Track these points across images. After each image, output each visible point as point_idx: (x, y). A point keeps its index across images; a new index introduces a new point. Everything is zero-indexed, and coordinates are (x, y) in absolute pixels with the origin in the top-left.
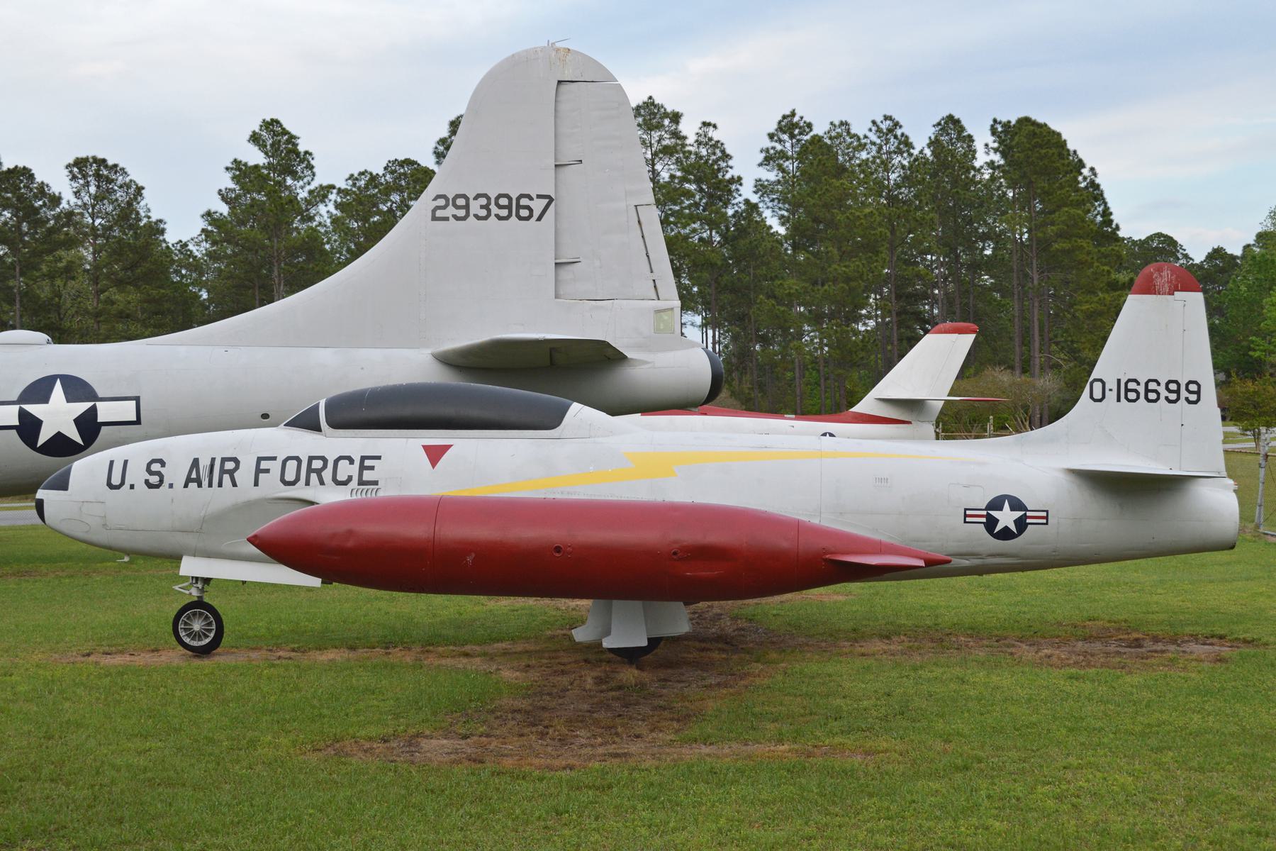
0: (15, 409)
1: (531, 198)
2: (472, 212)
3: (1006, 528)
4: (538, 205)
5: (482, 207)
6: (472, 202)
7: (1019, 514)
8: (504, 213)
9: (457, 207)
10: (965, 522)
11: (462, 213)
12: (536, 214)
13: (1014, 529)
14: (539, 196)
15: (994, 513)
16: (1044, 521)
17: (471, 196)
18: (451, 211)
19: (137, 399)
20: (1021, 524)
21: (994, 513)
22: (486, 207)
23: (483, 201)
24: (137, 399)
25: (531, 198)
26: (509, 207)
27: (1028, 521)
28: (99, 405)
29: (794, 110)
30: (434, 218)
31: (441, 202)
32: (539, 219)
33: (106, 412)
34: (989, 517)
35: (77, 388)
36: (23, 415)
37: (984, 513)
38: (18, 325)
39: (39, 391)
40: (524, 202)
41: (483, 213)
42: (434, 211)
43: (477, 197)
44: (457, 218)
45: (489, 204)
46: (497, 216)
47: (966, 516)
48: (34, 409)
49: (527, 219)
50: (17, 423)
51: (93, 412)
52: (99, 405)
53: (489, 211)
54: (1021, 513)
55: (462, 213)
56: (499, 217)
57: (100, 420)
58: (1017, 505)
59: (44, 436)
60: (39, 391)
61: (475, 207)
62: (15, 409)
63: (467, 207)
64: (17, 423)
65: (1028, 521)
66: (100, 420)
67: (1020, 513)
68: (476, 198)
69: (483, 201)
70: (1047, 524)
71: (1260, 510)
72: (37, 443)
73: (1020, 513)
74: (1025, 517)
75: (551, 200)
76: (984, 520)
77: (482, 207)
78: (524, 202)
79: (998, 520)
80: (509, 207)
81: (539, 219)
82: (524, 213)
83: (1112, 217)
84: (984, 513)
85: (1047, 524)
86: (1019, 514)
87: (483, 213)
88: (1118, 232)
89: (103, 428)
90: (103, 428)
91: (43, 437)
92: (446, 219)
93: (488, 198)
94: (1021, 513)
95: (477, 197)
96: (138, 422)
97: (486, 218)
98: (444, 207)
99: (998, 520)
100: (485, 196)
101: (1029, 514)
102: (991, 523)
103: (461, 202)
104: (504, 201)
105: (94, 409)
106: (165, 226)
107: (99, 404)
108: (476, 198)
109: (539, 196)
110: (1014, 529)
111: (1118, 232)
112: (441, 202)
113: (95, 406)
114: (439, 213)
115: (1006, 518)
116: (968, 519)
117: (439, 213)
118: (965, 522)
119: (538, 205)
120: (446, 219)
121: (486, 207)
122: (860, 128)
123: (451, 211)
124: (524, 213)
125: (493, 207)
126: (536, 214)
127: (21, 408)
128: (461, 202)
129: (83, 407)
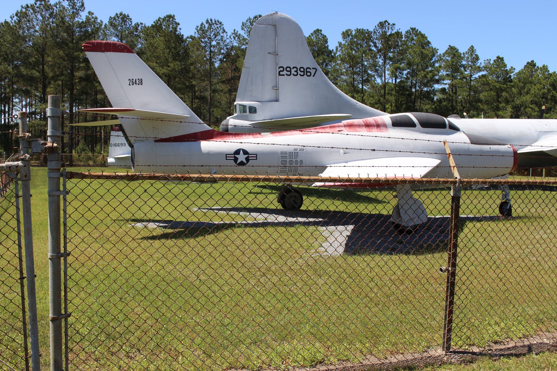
2: (292, 73)
3: (242, 162)
4: (313, 71)
5: (295, 71)
6: (292, 69)
7: (247, 156)
9: (288, 71)
10: (226, 159)
15: (237, 156)
16: (255, 158)
17: (292, 68)
20: (247, 159)
21: (237, 156)
22: (296, 71)
23: (295, 69)
26: (307, 72)
27: (250, 158)
30: (280, 75)
31: (282, 69)
32: (314, 76)
34: (235, 157)
37: (233, 156)
40: (308, 70)
41: (295, 73)
43: (294, 68)
44: (287, 75)
47: (226, 157)
49: (310, 76)
54: (247, 156)
55: (289, 73)
56: (301, 75)
58: (245, 152)
61: (293, 71)
63: (290, 71)
65: (250, 158)
67: (247, 156)
68: (293, 68)
69: (295, 69)
70: (256, 159)
71: (5, 116)
73: (247, 156)
74: (248, 157)
76: (233, 158)
77: (295, 71)
80: (304, 72)
81: (314, 76)
83: (344, 31)
84: (233, 156)
85: (256, 159)
86: (247, 156)
87: (295, 73)
89: (469, 229)
92: (284, 75)
93: (297, 69)
94: (247, 156)
95: (294, 68)
98: (283, 71)
100: (296, 67)
101: (250, 156)
102: (236, 160)
103: (288, 69)
108: (293, 68)
112: (282, 69)
114: (281, 73)
115: (242, 157)
116: (227, 158)
117: (281, 73)
118: (226, 159)
120: (284, 75)
121: (296, 71)
124: (309, 74)
125: (299, 71)
128: (288, 69)
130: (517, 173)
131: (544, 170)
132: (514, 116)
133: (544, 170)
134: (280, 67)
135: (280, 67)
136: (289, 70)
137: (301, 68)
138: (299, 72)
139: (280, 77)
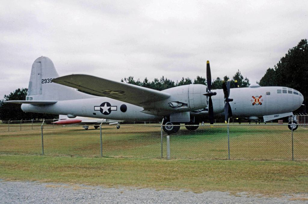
0: (99, 107)
11: (46, 82)
19: (117, 106)
22: (49, 81)
23: (48, 80)
24: (117, 106)
28: (111, 107)
30: (42, 83)
31: (43, 80)
33: (112, 108)
34: (101, 108)
35: (109, 105)
36: (101, 108)
38: (272, 84)
41: (48, 82)
43: (48, 79)
48: (102, 107)
50: (100, 109)
51: (110, 108)
52: (111, 107)
55: (46, 82)
59: (104, 112)
60: (103, 105)
62: (99, 107)
63: (46, 81)
64: (100, 109)
69: (48, 80)
87: (48, 82)
88: (285, 57)
89: (112, 111)
91: (104, 112)
95: (48, 79)
96: (117, 110)
98: (43, 81)
106: (276, 66)
111: (285, 57)
112: (43, 80)
114: (43, 82)
117: (43, 82)
121: (49, 81)
123: (44, 82)
125: (50, 81)
128: (46, 80)
129: (109, 107)
130: (292, 49)
131: (207, 112)
132: (272, 84)
133: (207, 112)
134: (42, 80)
135: (42, 80)
136: (46, 80)
137: (51, 79)
138: (50, 81)
139: (117, 110)
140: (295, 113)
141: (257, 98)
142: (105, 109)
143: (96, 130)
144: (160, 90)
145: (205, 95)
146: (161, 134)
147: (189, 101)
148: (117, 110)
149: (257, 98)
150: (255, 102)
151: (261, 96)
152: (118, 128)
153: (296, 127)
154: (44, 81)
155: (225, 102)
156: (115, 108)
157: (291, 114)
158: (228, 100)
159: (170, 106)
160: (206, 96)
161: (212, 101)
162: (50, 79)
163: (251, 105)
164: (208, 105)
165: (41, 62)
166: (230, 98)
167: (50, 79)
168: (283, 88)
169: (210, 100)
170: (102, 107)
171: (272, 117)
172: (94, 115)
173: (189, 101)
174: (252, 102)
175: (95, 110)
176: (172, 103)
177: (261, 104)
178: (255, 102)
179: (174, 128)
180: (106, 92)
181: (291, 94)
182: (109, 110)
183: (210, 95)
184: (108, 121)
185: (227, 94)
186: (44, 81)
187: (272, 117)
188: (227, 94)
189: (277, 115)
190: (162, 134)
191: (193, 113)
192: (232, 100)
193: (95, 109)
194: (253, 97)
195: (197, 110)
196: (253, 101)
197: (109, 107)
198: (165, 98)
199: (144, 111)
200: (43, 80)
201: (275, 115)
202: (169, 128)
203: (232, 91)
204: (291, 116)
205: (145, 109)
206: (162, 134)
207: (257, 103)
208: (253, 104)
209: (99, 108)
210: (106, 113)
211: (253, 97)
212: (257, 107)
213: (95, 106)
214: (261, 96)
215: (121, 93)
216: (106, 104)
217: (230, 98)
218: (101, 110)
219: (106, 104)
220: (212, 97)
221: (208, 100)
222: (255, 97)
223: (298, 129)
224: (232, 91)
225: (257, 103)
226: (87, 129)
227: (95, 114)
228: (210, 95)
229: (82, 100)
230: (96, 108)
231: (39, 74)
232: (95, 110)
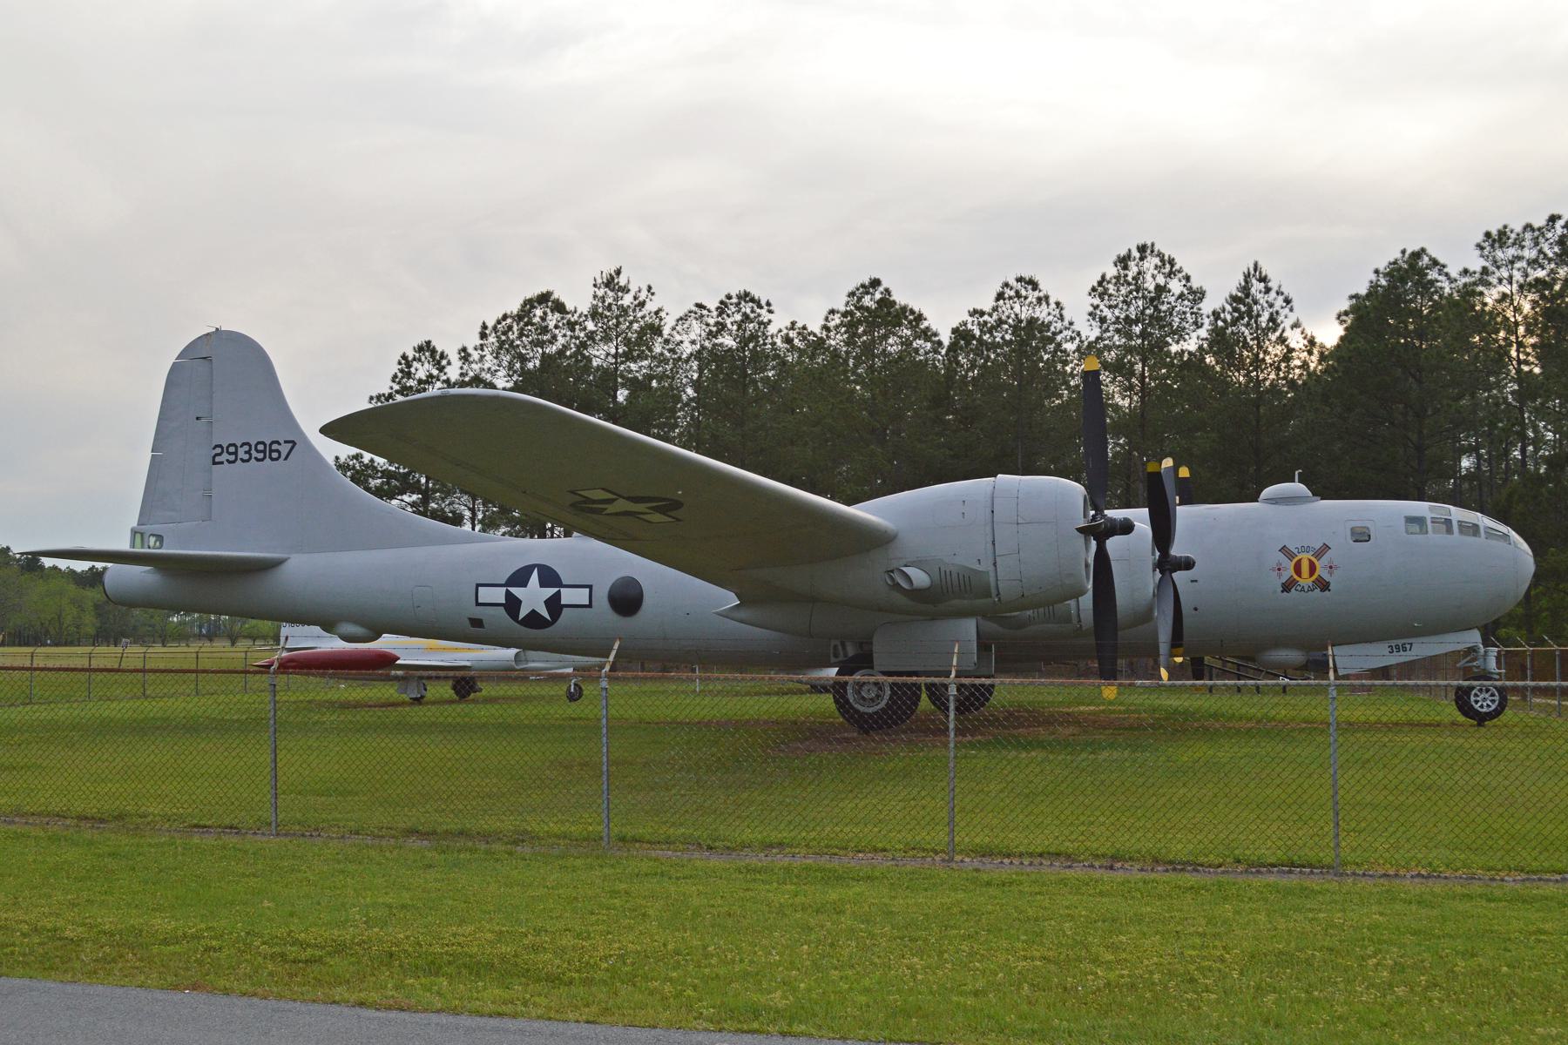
1: (279, 444)
4: (284, 449)
5: (246, 452)
8: (260, 456)
9: (230, 454)
11: (232, 458)
12: (283, 456)
13: (545, 614)
14: (286, 442)
17: (239, 445)
18: (225, 457)
23: (246, 448)
24: (590, 587)
25: (279, 444)
29: (484, 323)
31: (218, 450)
32: (286, 459)
33: (568, 596)
35: (549, 577)
36: (509, 595)
39: (520, 578)
40: (275, 447)
41: (246, 457)
42: (214, 457)
43: (243, 444)
45: (250, 449)
46: (256, 458)
48: (514, 590)
51: (558, 595)
53: (250, 455)
55: (232, 458)
56: (257, 459)
57: (562, 603)
59: (523, 613)
60: (520, 578)
61: (242, 454)
63: (236, 453)
66: (562, 603)
69: (246, 448)
72: (518, 616)
75: (294, 443)
77: (246, 452)
78: (275, 447)
79: (533, 611)
80: (264, 452)
81: (286, 459)
82: (275, 455)
87: (246, 457)
89: (565, 609)
90: (565, 609)
91: (523, 613)
92: (222, 463)
95: (243, 444)
96: (590, 606)
97: (248, 461)
98: (220, 454)
99: (533, 611)
100: (248, 444)
103: (232, 449)
104: (261, 447)
105: (558, 595)
107: (562, 589)
109: (286, 442)
110: (545, 614)
112: (218, 450)
113: (559, 592)
114: (217, 459)
117: (217, 459)
119: (284, 449)
120: (222, 463)
122: (671, 304)
123: (225, 457)
125: (253, 452)
126: (283, 456)
127: (507, 591)
128: (232, 449)
129: (553, 591)
135: (216, 446)
140: (1490, 633)
141: (1305, 558)
142: (533, 596)
143: (460, 707)
144: (849, 502)
145: (1080, 530)
146: (947, 729)
147: (995, 564)
148: (590, 606)
149: (1305, 558)
150: (1296, 577)
151: (1326, 547)
152: (574, 697)
153: (1497, 698)
154: (226, 453)
155: (1154, 570)
156: (581, 596)
157: (1474, 638)
158: (1167, 564)
159: (897, 586)
160: (1081, 538)
161: (1113, 563)
162: (268, 443)
163: (1275, 592)
164: (1090, 586)
165: (214, 359)
166: (1176, 551)
167: (268, 443)
168: (1431, 509)
169: (1102, 558)
170: (514, 590)
171: (1379, 655)
172: (475, 631)
173: (995, 564)
174: (1280, 576)
175: (478, 604)
176: (904, 569)
177: (1324, 586)
178: (1296, 577)
179: (894, 693)
180: (588, 500)
181: (1476, 539)
182: (554, 604)
183: (1100, 532)
184: (527, 661)
185: (1163, 530)
186: (226, 453)
187: (1379, 655)
188: (1163, 530)
189: (1400, 642)
190: (952, 726)
191: (991, 627)
192: (1188, 564)
193: (480, 601)
194: (1284, 550)
195: (1008, 614)
196: (1286, 569)
197: (553, 591)
198: (872, 540)
199: (742, 614)
200: (220, 446)
201: (1394, 642)
202: (872, 700)
203: (1186, 515)
204: (1472, 650)
205: (745, 601)
206: (952, 726)
207: (1306, 580)
208: (1287, 587)
209: (498, 595)
210: (534, 620)
211: (1284, 550)
212: (1305, 600)
213: (478, 585)
214: (1326, 547)
215: (656, 509)
216: (535, 573)
217: (1176, 551)
218: (512, 604)
219: (535, 573)
220: (1114, 544)
221: (1091, 561)
222: (1296, 551)
223: (1503, 718)
224: (1186, 515)
225: (1306, 580)
226: (418, 701)
227: (477, 623)
228: (1100, 532)
229: (419, 554)
230: (487, 595)
231: (197, 418)
232: (478, 604)
